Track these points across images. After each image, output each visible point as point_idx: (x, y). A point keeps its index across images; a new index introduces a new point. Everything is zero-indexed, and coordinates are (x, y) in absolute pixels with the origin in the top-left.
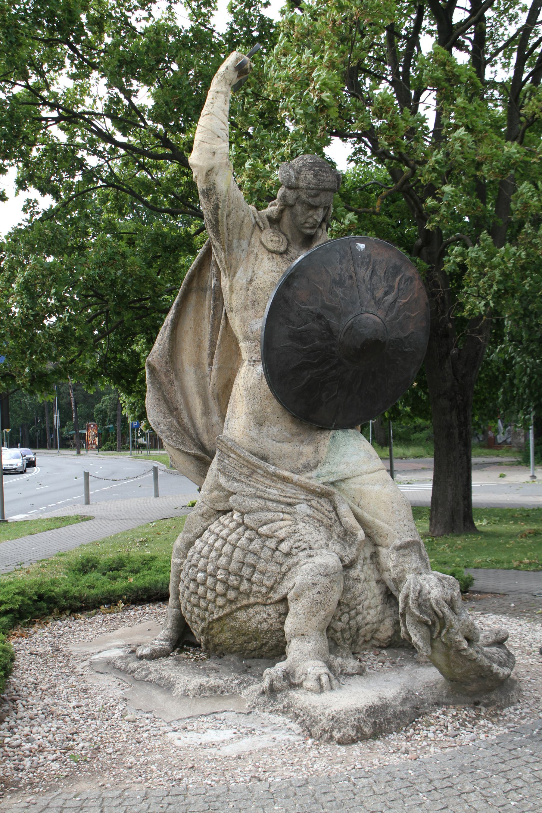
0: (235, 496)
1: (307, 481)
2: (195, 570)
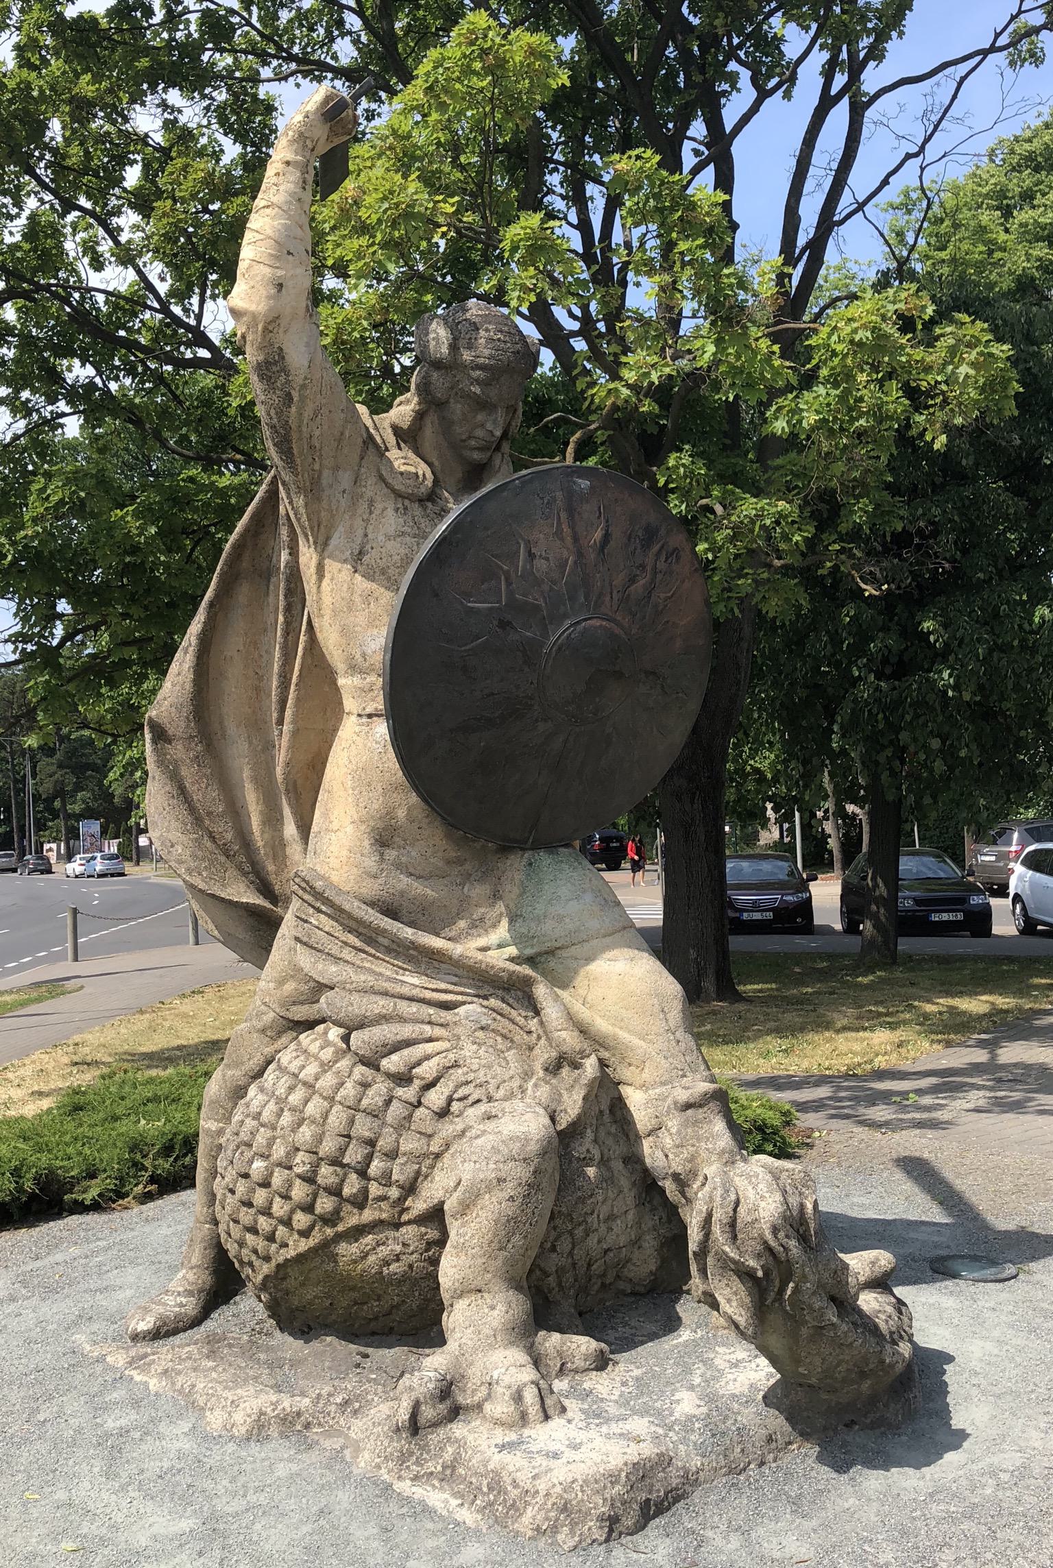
0: (330, 994)
1: (480, 956)
2: (248, 1154)
